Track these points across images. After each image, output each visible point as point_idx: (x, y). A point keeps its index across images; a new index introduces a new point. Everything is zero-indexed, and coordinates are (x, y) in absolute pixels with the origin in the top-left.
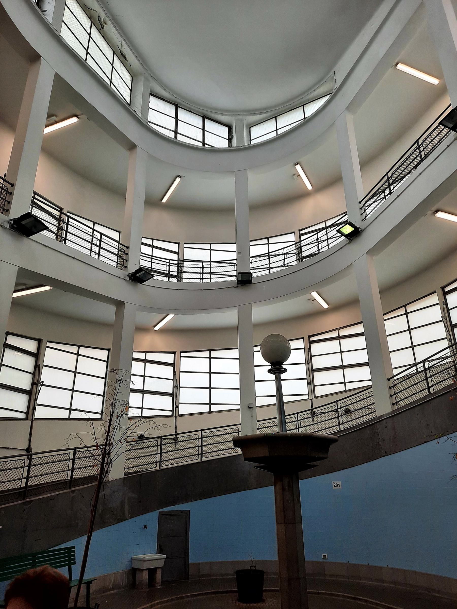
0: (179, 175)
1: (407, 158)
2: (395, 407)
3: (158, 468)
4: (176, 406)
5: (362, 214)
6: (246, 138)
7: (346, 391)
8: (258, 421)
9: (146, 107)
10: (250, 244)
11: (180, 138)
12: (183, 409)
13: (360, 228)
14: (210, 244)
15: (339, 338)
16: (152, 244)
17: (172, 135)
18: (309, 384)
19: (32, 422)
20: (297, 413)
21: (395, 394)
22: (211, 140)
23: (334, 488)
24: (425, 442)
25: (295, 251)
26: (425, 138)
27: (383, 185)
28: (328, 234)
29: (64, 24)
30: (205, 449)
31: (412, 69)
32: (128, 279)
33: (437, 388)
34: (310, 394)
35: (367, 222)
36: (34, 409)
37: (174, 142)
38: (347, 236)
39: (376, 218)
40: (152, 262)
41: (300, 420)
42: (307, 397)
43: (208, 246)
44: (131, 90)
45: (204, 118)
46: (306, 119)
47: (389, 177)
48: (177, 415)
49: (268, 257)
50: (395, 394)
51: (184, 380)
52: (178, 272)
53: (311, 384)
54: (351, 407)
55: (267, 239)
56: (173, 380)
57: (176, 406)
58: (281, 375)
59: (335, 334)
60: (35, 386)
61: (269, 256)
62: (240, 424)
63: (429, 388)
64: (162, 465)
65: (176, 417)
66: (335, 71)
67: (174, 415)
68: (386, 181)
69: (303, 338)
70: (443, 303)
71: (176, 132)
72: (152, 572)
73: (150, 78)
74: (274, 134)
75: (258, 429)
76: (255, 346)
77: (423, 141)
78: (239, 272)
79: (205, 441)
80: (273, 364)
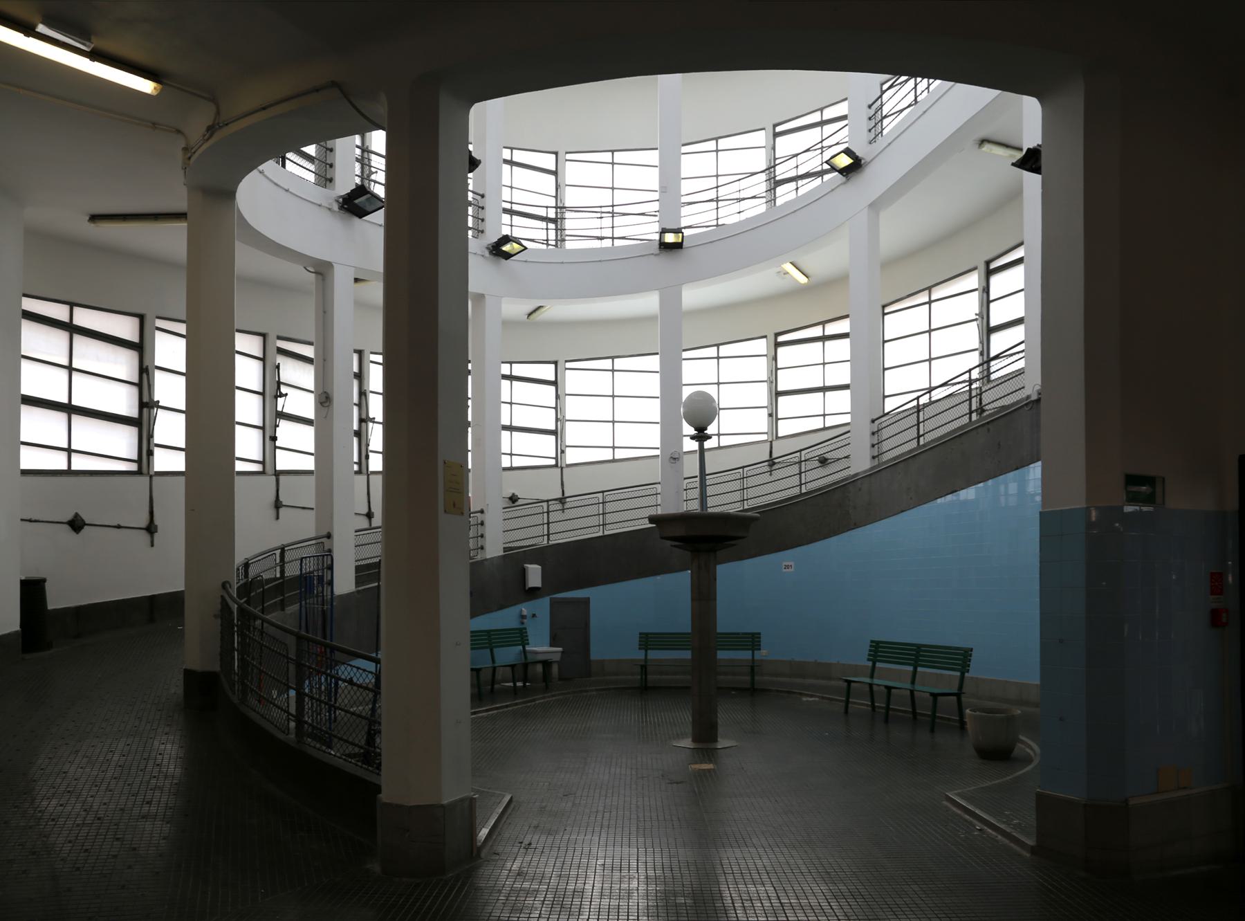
2: (876, 462)
3: (600, 534)
4: (561, 451)
5: (870, 130)
7: (825, 429)
8: (685, 479)
10: (682, 152)
12: (572, 457)
13: (864, 159)
14: (613, 151)
15: (824, 338)
18: (770, 415)
19: (368, 475)
20: (743, 467)
21: (878, 443)
23: (784, 570)
24: (902, 511)
30: (609, 519)
32: (487, 253)
33: (929, 437)
34: (770, 433)
35: (881, 142)
36: (367, 457)
41: (747, 477)
42: (764, 437)
43: (607, 157)
48: (564, 465)
50: (878, 443)
51: (573, 408)
53: (773, 416)
54: (827, 456)
55: (714, 142)
56: (556, 408)
57: (561, 451)
58: (705, 443)
59: (816, 332)
60: (363, 424)
62: (659, 483)
63: (919, 437)
64: (551, 539)
65: (562, 468)
67: (559, 465)
69: (765, 337)
70: (984, 290)
72: (547, 664)
75: (685, 490)
76: (684, 350)
79: (609, 507)
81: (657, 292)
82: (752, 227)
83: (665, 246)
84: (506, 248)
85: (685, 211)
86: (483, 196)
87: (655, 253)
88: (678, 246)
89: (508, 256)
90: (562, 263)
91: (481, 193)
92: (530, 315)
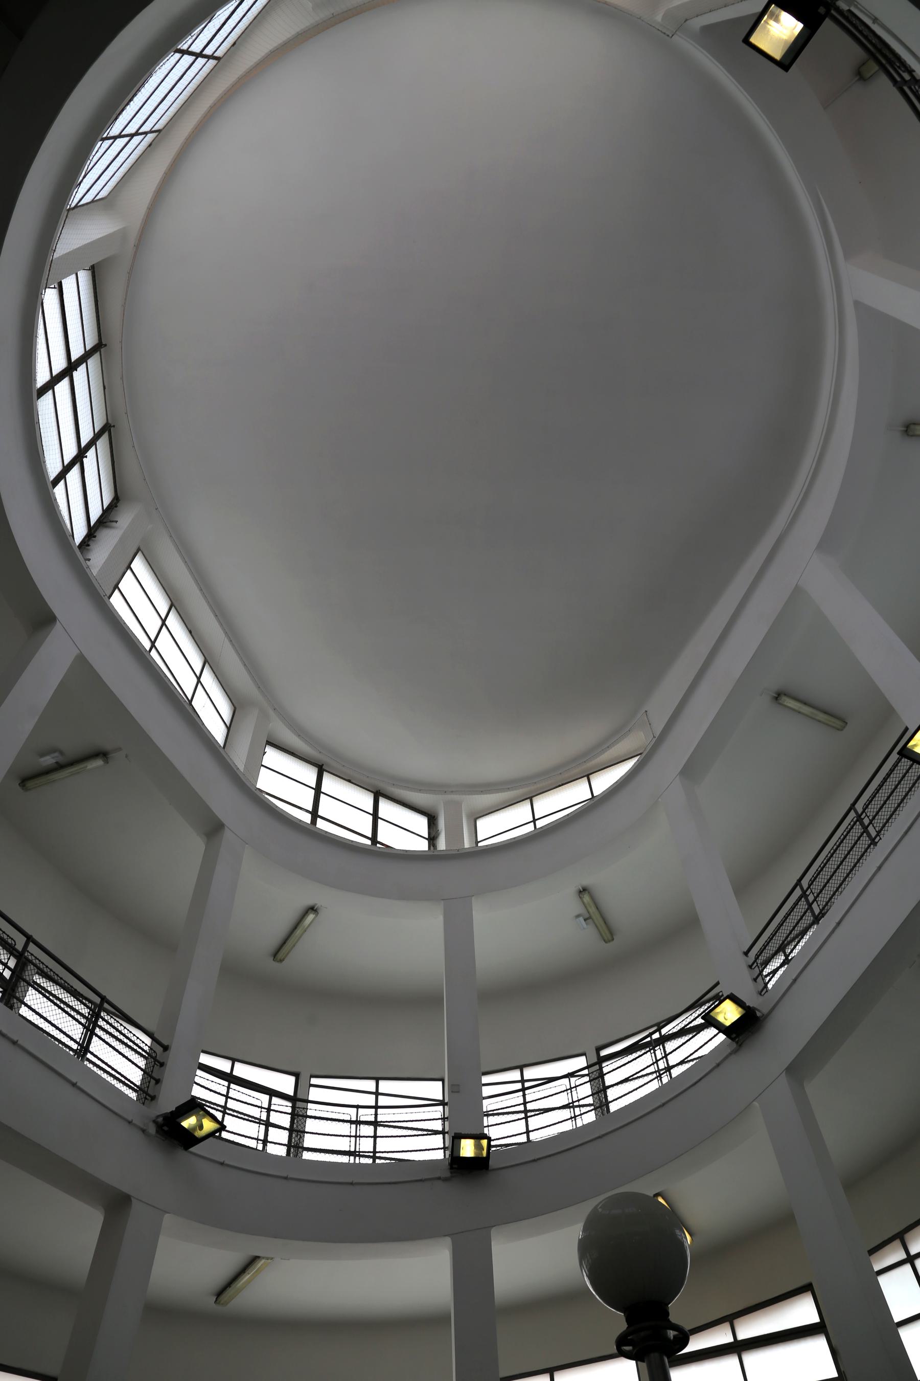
0: (317, 903)
1: (838, 843)
5: (755, 980)
6: (466, 830)
9: (256, 764)
11: (321, 824)
13: (759, 1011)
16: (229, 1071)
17: (307, 818)
22: (388, 836)
25: (590, 1100)
26: (876, 789)
27: (794, 908)
28: (668, 1057)
29: (125, 130)
31: (558, 1212)
32: (152, 1129)
37: (309, 832)
38: (729, 1031)
39: (795, 980)
40: (227, 1097)
44: (229, 728)
45: (378, 795)
46: (595, 799)
47: (805, 889)
49: (523, 1115)
52: (289, 1146)
61: (526, 1111)
66: (646, 711)
68: (799, 899)
71: (315, 814)
73: (271, 712)
74: (530, 828)
77: (866, 806)
78: (455, 1134)
80: (633, 1313)
81: (448, 1240)
82: (597, 1135)
83: (456, 1163)
84: (189, 1123)
85: (485, 1102)
86: (166, 1048)
87: (443, 1176)
88: (478, 1165)
89: (188, 1139)
90: (286, 1178)
91: (165, 1043)
92: (220, 1294)
